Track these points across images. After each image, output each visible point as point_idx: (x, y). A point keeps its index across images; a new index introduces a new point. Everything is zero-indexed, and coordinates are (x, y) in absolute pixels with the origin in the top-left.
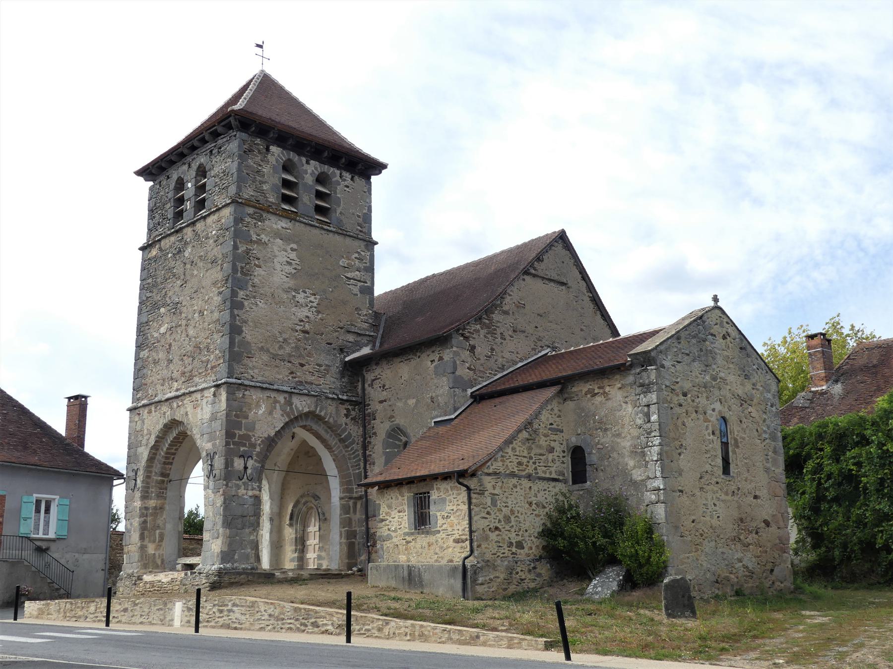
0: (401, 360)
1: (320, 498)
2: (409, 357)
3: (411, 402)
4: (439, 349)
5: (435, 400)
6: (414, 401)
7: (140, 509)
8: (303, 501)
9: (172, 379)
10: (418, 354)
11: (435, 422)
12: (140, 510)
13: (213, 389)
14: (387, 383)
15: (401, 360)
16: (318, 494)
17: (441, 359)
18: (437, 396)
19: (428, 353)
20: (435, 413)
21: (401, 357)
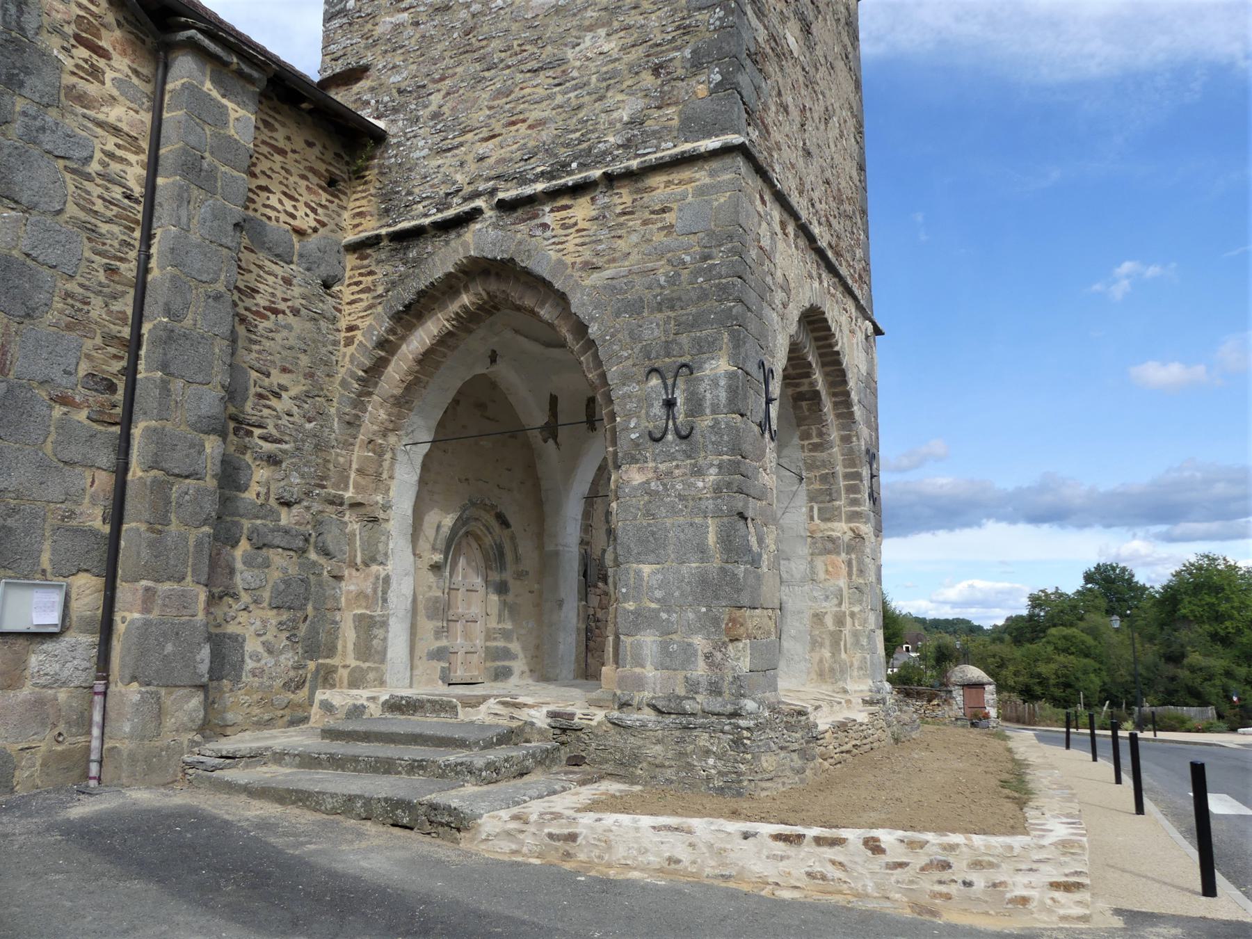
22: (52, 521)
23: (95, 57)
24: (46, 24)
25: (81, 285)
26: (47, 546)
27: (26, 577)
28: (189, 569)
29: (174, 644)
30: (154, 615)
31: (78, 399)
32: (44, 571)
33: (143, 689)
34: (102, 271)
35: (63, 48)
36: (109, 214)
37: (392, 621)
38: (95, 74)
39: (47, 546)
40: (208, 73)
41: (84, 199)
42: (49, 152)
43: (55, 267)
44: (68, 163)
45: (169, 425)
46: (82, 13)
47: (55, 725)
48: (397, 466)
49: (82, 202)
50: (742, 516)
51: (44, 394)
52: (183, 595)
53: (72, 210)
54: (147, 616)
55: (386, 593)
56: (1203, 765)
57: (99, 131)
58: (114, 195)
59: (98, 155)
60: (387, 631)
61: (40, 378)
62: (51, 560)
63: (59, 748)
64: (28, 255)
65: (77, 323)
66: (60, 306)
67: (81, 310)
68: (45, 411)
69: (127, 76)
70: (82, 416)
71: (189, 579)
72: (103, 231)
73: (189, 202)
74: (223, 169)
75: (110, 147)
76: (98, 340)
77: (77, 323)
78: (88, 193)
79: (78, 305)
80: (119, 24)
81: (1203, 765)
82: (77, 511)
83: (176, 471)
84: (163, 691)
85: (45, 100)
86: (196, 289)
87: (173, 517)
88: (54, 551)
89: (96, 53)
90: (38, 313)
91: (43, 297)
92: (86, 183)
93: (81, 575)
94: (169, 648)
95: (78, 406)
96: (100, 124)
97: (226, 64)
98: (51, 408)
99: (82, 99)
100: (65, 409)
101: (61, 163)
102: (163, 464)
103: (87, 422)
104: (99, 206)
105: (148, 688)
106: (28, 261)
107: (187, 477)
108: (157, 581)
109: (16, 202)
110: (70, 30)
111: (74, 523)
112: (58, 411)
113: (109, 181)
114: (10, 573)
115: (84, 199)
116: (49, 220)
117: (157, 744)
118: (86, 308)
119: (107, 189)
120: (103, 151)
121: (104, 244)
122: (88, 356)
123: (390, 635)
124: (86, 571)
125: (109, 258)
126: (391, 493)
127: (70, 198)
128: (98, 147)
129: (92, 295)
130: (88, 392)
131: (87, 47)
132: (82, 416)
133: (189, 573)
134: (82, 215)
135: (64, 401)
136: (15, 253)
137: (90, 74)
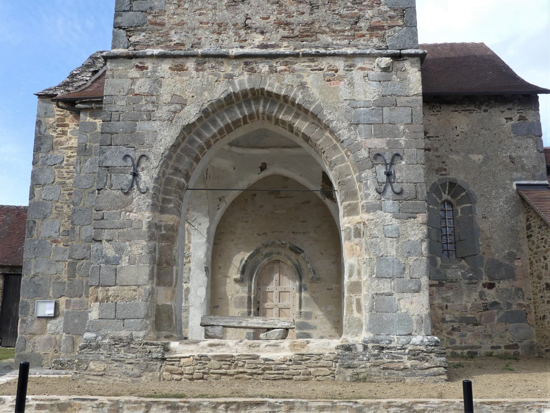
0: (454, 109)
1: (303, 251)
2: (457, 109)
3: (477, 158)
4: (519, 108)
5: (517, 161)
6: (481, 157)
7: (150, 225)
8: (267, 251)
9: (246, 27)
10: (484, 108)
11: (517, 185)
12: (149, 227)
13: (385, 61)
14: (431, 130)
15: (454, 109)
16: (299, 245)
17: (522, 118)
18: (521, 157)
19: (502, 109)
20: (515, 175)
21: (455, 105)
22: (53, 280)
23: (64, 128)
24: (47, 127)
25: (61, 203)
26: (51, 289)
27: (45, 299)
28: (84, 292)
29: (78, 320)
30: (70, 310)
31: (59, 240)
32: (50, 297)
33: (67, 335)
34: (67, 196)
35: (53, 131)
36: (69, 176)
37: (191, 309)
38: (64, 133)
39: (51, 289)
40: (88, 114)
41: (61, 175)
42: (49, 165)
43: (52, 200)
44: (56, 166)
45: (74, 242)
46: (59, 117)
47: (55, 347)
48: (192, 237)
49: (60, 176)
50: (294, 226)
51: (49, 241)
52: (81, 302)
53: (57, 180)
54: (68, 310)
55: (187, 296)
56: (29, 363)
57: (66, 151)
58: (71, 169)
59: (66, 158)
60: (189, 314)
61: (48, 236)
62: (52, 293)
63: (56, 355)
64: (44, 199)
65: (60, 214)
66: (54, 212)
67: (60, 211)
68: (50, 246)
69: (74, 128)
70: (61, 245)
71: (84, 296)
72: (67, 183)
73: (81, 163)
74: (95, 145)
75: (70, 154)
76: (66, 219)
77: (60, 214)
78: (62, 172)
79: (60, 209)
80: (71, 113)
81: (29, 363)
82: (61, 276)
83: (78, 258)
84: (75, 336)
85: (48, 150)
86: (84, 192)
87: (77, 275)
88: (53, 290)
89: (64, 127)
90: (48, 216)
91: (49, 211)
92: (61, 170)
93: (63, 297)
94: (76, 321)
95: (60, 242)
96: (66, 149)
97: (92, 108)
98: (52, 245)
99: (61, 143)
100: (55, 244)
101: (54, 167)
102: (73, 257)
103: (63, 247)
104: (65, 175)
105: (69, 335)
106: (45, 201)
107: (82, 259)
108: (71, 297)
109: (40, 185)
110: (55, 125)
111: (60, 280)
112: (54, 244)
113: (69, 166)
114: (40, 298)
115: (61, 175)
116: (50, 187)
117: (73, 355)
118: (62, 209)
119: (68, 168)
120: (67, 157)
121: (68, 187)
122: (63, 225)
123: (191, 316)
124: (64, 296)
125: (69, 190)
126: (191, 250)
127: (56, 177)
128: (65, 155)
129: (63, 205)
130: (63, 237)
131: (61, 126)
132: (61, 245)
133: (84, 294)
134: (61, 180)
135: (55, 241)
136: (40, 200)
137: (62, 134)
